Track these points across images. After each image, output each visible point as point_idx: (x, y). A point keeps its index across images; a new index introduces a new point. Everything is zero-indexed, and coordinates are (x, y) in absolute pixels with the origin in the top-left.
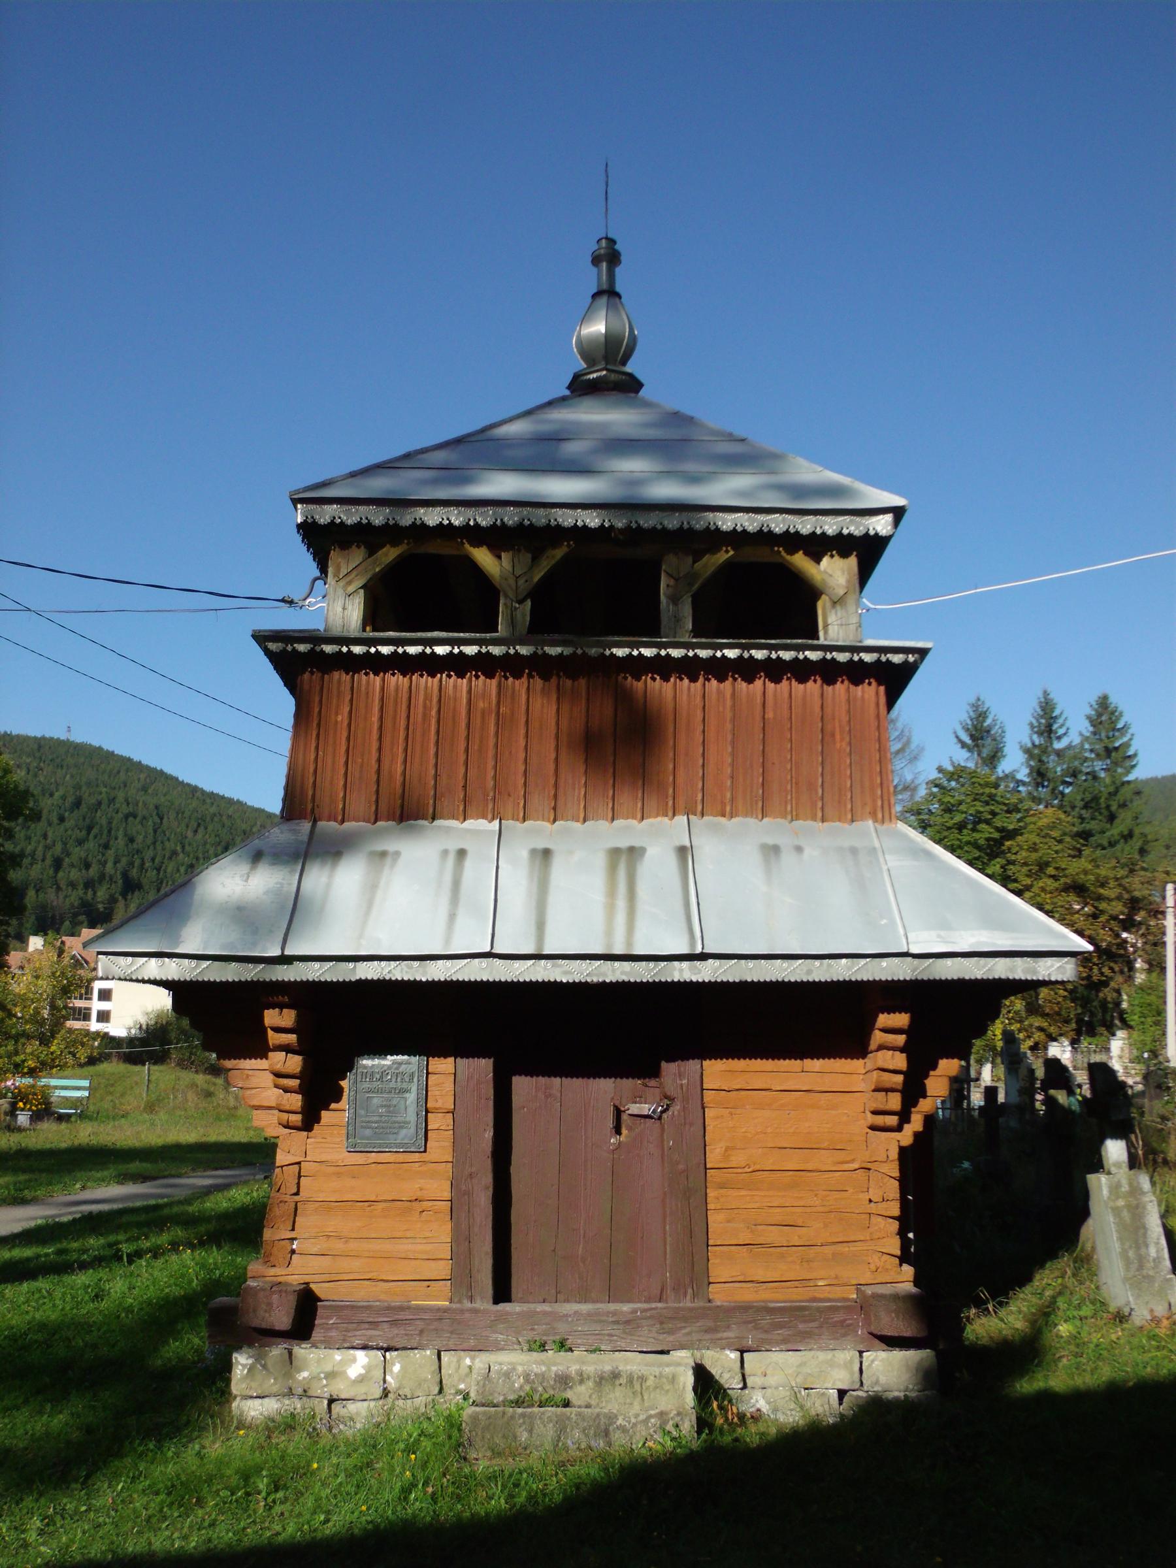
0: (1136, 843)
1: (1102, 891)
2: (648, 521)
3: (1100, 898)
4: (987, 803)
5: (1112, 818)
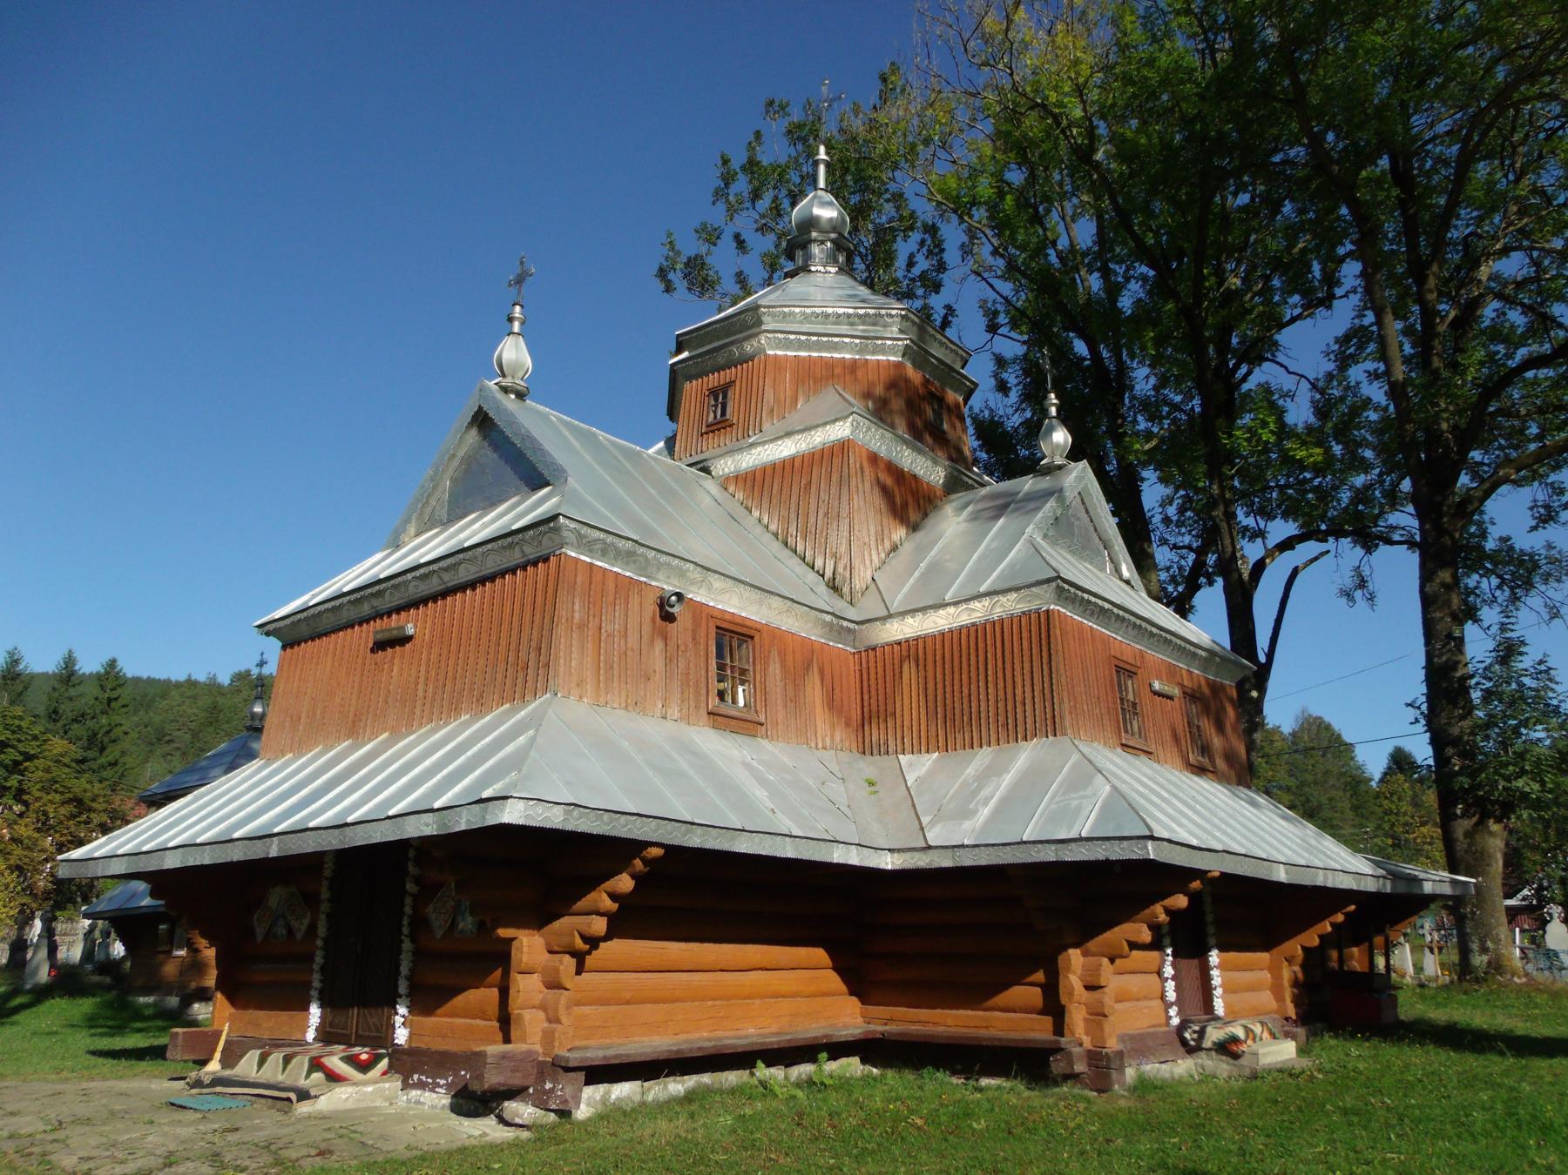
0: (119, 768)
1: (94, 805)
2: (312, 611)
3: (90, 810)
4: (13, 732)
5: (102, 749)
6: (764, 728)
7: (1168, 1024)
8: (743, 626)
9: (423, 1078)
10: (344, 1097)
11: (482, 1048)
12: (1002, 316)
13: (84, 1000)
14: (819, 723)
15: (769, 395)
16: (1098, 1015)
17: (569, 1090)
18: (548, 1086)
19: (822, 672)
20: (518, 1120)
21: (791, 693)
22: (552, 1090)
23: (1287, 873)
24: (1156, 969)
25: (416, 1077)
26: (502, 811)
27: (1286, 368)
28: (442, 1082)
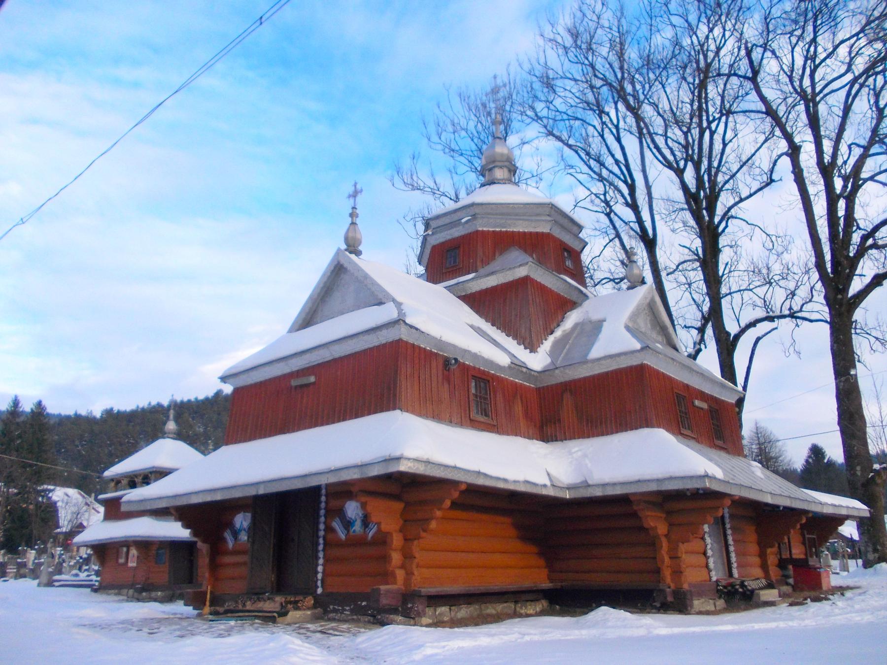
6: (496, 427)
7: (710, 580)
8: (160, 498)
9: (336, 607)
10: (298, 616)
11: (377, 587)
14: (522, 424)
15: (480, 253)
16: (678, 573)
17: (421, 608)
18: (409, 605)
19: (521, 397)
21: (507, 408)
22: (412, 608)
23: (772, 499)
24: (702, 551)
25: (331, 607)
26: (399, 466)
27: (747, 222)
28: (348, 608)
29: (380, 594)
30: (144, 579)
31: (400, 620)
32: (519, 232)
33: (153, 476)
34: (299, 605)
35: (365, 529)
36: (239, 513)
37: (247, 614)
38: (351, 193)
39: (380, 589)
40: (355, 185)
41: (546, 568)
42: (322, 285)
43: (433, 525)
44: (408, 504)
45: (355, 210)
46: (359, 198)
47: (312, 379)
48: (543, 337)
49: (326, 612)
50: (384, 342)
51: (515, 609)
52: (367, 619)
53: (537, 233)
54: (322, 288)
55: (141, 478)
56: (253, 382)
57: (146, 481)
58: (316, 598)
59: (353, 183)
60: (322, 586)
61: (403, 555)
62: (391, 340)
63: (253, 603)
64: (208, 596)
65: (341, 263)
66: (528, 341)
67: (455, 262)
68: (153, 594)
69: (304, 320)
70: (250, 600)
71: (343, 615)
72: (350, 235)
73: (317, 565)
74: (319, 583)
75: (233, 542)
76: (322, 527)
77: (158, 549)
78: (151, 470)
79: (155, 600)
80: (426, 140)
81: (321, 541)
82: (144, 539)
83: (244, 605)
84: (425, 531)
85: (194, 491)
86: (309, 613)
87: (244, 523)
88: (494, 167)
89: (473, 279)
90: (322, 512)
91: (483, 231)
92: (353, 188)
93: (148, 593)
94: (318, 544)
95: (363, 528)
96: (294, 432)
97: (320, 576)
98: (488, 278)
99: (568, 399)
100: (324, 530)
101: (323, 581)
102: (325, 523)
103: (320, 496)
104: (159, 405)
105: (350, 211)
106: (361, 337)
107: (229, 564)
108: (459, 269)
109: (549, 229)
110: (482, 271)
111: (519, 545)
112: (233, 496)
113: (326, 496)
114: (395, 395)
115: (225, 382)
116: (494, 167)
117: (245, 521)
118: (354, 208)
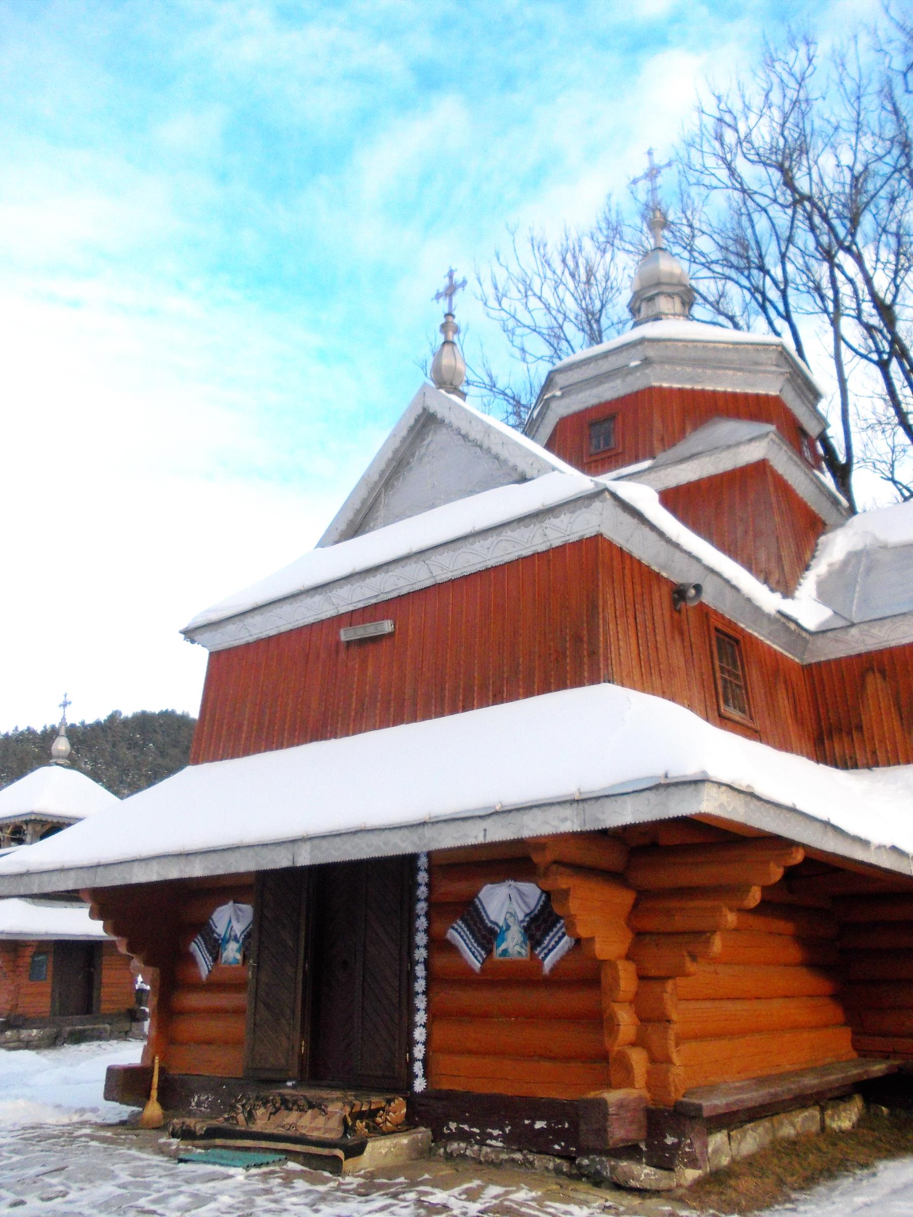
8: (63, 870)
9: (466, 1127)
11: (592, 1095)
12: (250, 689)
13: (619, 1017)
15: (657, 424)
19: (785, 682)
20: (633, 1183)
22: (676, 1146)
28: (496, 1133)
29: (606, 1115)
30: (8, 1007)
31: (647, 1175)
32: (725, 394)
33: (30, 827)
34: (379, 1120)
35: (533, 948)
36: (224, 903)
37: (264, 1144)
38: (442, 290)
39: (601, 1104)
40: (451, 275)
41: (845, 1024)
42: (390, 455)
43: (717, 944)
44: (644, 896)
45: (450, 318)
46: (457, 298)
47: (387, 626)
48: (798, 573)
49: (439, 1137)
50: (557, 543)
51: (823, 1121)
52: (552, 1163)
53: (757, 397)
54: (390, 461)
55: (8, 831)
56: (251, 639)
57: (18, 836)
58: (412, 1100)
59: (447, 271)
60: (425, 1075)
61: (638, 1013)
62: (574, 538)
63: (274, 1113)
64: (155, 1080)
65: (431, 411)
66: (776, 576)
67: (607, 443)
68: (24, 1034)
69: (351, 523)
70: (265, 1104)
71: (486, 1149)
72: (446, 361)
73: (412, 1026)
74: (418, 1068)
75: (210, 963)
76: (421, 939)
77: (38, 953)
78: (28, 818)
79: (28, 1045)
80: (481, 304)
81: (420, 971)
82: (10, 938)
83: (250, 1117)
84: (694, 958)
85: (138, 857)
86: (405, 1141)
87: (234, 923)
88: (657, 294)
89: (650, 469)
90: (422, 907)
91: (660, 389)
92: (446, 281)
93: (15, 1031)
94: (413, 978)
95: (528, 949)
96: (347, 735)
97: (419, 1051)
98: (684, 466)
99: (874, 683)
100: (427, 947)
101: (425, 1061)
102: (427, 931)
103: (416, 870)
104: (30, 731)
105: (443, 320)
106: (508, 533)
107: (196, 1011)
108: (615, 455)
109: (779, 388)
110: (662, 457)
111: (806, 980)
112: (233, 870)
113: (429, 871)
114: (593, 653)
115: (193, 641)
116: (657, 294)
117: (238, 920)
118: (449, 315)
